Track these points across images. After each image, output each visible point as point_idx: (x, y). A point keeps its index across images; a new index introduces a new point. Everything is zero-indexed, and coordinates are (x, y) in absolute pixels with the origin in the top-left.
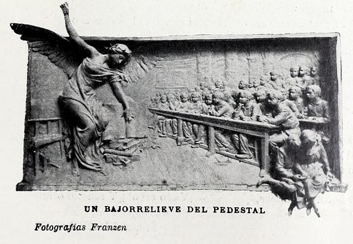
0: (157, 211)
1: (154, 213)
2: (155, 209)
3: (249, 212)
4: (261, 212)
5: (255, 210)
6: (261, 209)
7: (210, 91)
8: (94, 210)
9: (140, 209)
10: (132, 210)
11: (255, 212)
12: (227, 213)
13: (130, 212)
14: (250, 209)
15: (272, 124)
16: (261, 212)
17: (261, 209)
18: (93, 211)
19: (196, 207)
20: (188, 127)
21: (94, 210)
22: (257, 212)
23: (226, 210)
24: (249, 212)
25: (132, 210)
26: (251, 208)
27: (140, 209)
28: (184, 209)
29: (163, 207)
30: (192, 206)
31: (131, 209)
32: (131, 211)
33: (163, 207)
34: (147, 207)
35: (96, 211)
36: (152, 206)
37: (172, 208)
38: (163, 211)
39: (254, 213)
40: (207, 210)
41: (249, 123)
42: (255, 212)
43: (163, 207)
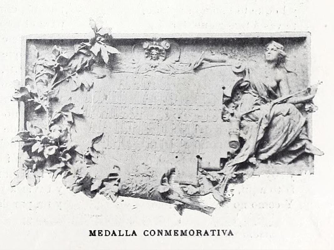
0: (125, 234)
1: (147, 236)
2: (123, 232)
3: (213, 235)
4: (120, 235)
5: (206, 232)
6: (120, 231)
7: (44, 60)
8: (159, 233)
9: (199, 233)
10: (199, 234)
11: (230, 234)
12: (126, 236)
13: (197, 235)
14: (214, 231)
15: (219, 62)
16: (120, 235)
17: (120, 231)
18: (158, 235)
19: (223, 231)
20: (202, 55)
21: (159, 233)
22: (115, 235)
23: (104, 233)
24: (213, 235)
25: (199, 234)
26: (215, 230)
27: (199, 233)
28: (139, 233)
29: (99, 231)
30: (109, 231)
31: (198, 233)
32: (198, 235)
33: (99, 231)
34: (101, 231)
35: (91, 231)
36: (126, 230)
37: (225, 231)
38: (175, 235)
39: (229, 235)
40: (123, 233)
41: (43, 139)
42: (230, 234)
43: (175, 231)
